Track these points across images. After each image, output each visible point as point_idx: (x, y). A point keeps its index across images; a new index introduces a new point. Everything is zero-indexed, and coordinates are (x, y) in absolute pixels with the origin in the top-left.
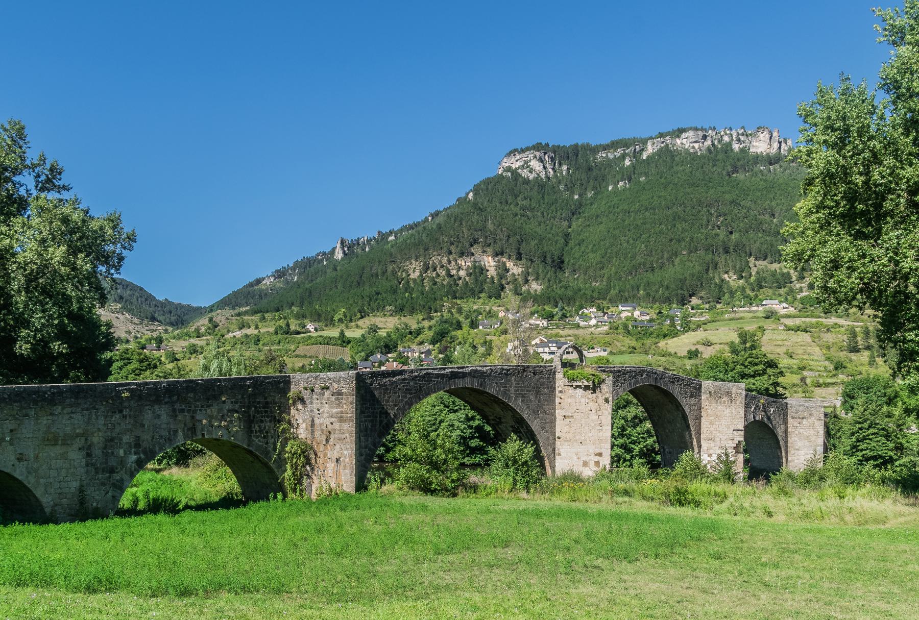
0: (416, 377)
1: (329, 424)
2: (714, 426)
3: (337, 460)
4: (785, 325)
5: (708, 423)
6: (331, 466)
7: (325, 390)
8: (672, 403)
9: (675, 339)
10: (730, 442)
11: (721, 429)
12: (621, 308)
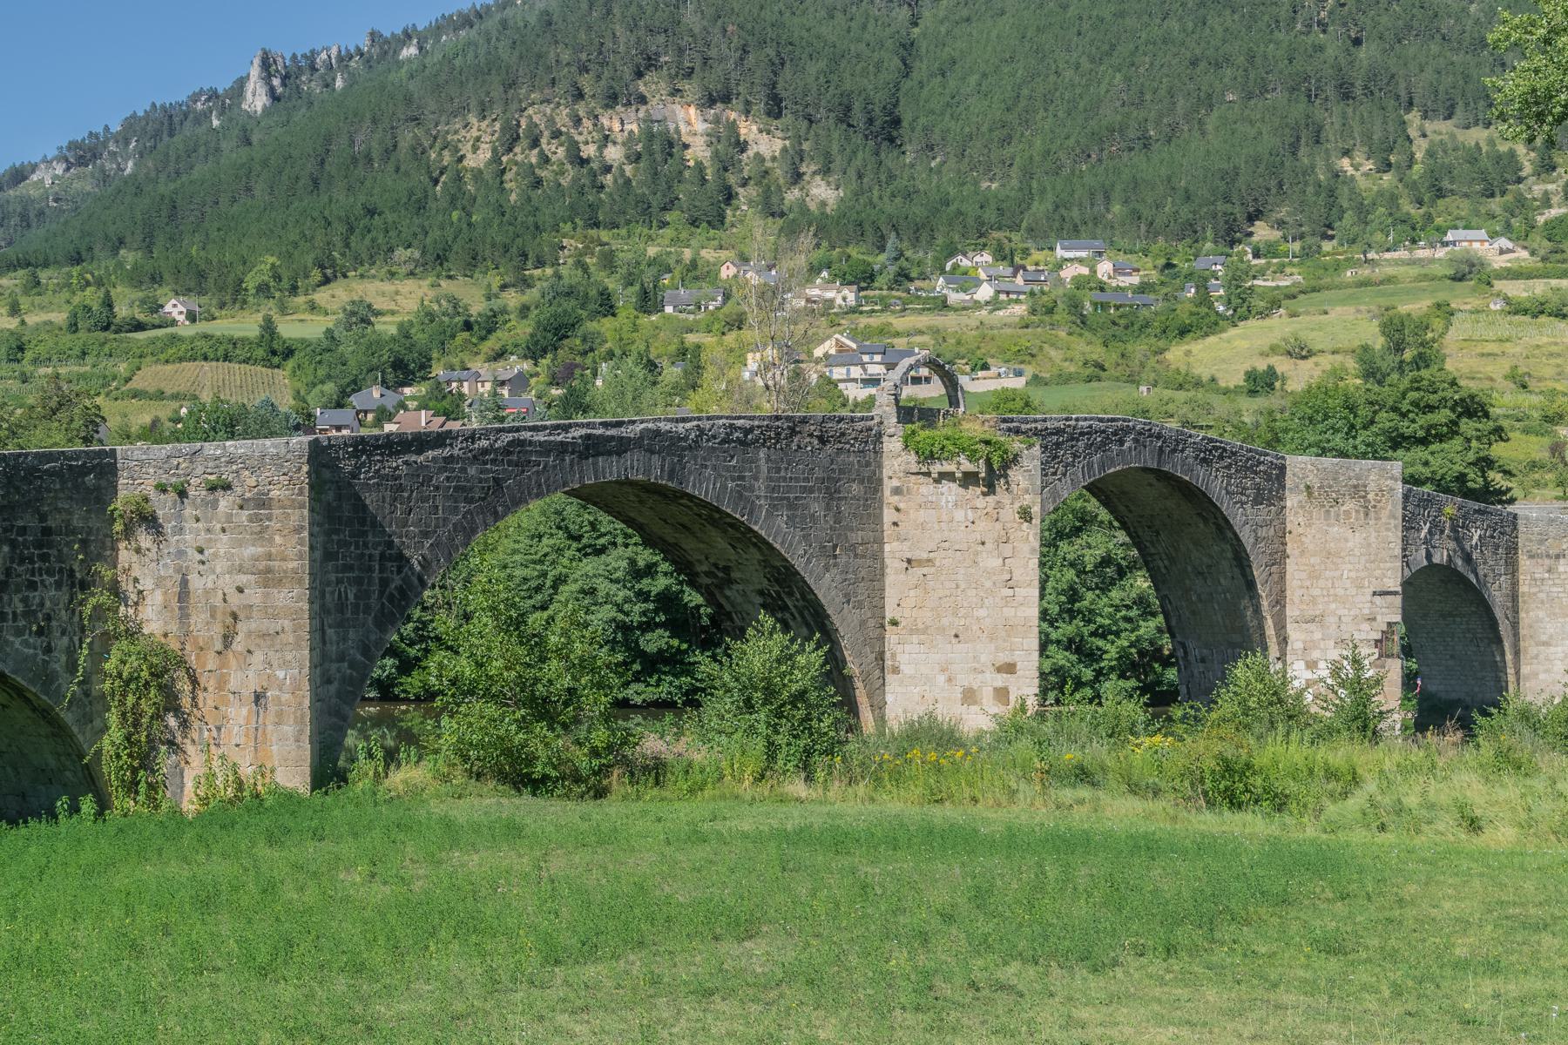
0: (485, 451)
1: (230, 591)
2: (1321, 583)
4: (1507, 301)
5: (1304, 575)
6: (239, 714)
7: (220, 493)
8: (1205, 520)
9: (1212, 339)
10: (1366, 626)
11: (1341, 592)
12: (1060, 253)
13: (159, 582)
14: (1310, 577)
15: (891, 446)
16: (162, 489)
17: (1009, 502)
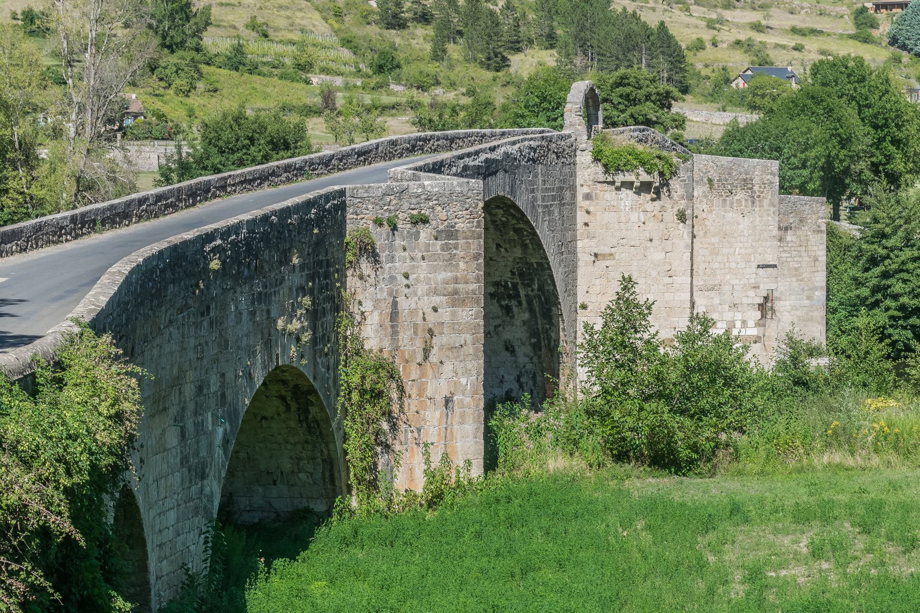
1: (429, 311)
2: (719, 258)
3: (448, 401)
5: (707, 252)
6: (433, 416)
7: (420, 226)
10: (751, 293)
11: (733, 265)
13: (377, 303)
14: (711, 254)
15: (582, 159)
16: (379, 223)
17: (670, 206)
